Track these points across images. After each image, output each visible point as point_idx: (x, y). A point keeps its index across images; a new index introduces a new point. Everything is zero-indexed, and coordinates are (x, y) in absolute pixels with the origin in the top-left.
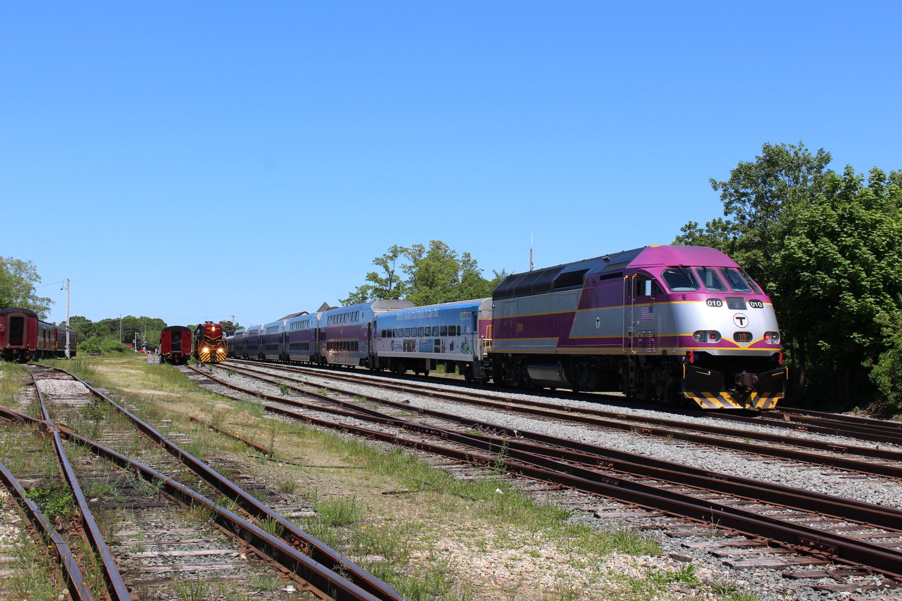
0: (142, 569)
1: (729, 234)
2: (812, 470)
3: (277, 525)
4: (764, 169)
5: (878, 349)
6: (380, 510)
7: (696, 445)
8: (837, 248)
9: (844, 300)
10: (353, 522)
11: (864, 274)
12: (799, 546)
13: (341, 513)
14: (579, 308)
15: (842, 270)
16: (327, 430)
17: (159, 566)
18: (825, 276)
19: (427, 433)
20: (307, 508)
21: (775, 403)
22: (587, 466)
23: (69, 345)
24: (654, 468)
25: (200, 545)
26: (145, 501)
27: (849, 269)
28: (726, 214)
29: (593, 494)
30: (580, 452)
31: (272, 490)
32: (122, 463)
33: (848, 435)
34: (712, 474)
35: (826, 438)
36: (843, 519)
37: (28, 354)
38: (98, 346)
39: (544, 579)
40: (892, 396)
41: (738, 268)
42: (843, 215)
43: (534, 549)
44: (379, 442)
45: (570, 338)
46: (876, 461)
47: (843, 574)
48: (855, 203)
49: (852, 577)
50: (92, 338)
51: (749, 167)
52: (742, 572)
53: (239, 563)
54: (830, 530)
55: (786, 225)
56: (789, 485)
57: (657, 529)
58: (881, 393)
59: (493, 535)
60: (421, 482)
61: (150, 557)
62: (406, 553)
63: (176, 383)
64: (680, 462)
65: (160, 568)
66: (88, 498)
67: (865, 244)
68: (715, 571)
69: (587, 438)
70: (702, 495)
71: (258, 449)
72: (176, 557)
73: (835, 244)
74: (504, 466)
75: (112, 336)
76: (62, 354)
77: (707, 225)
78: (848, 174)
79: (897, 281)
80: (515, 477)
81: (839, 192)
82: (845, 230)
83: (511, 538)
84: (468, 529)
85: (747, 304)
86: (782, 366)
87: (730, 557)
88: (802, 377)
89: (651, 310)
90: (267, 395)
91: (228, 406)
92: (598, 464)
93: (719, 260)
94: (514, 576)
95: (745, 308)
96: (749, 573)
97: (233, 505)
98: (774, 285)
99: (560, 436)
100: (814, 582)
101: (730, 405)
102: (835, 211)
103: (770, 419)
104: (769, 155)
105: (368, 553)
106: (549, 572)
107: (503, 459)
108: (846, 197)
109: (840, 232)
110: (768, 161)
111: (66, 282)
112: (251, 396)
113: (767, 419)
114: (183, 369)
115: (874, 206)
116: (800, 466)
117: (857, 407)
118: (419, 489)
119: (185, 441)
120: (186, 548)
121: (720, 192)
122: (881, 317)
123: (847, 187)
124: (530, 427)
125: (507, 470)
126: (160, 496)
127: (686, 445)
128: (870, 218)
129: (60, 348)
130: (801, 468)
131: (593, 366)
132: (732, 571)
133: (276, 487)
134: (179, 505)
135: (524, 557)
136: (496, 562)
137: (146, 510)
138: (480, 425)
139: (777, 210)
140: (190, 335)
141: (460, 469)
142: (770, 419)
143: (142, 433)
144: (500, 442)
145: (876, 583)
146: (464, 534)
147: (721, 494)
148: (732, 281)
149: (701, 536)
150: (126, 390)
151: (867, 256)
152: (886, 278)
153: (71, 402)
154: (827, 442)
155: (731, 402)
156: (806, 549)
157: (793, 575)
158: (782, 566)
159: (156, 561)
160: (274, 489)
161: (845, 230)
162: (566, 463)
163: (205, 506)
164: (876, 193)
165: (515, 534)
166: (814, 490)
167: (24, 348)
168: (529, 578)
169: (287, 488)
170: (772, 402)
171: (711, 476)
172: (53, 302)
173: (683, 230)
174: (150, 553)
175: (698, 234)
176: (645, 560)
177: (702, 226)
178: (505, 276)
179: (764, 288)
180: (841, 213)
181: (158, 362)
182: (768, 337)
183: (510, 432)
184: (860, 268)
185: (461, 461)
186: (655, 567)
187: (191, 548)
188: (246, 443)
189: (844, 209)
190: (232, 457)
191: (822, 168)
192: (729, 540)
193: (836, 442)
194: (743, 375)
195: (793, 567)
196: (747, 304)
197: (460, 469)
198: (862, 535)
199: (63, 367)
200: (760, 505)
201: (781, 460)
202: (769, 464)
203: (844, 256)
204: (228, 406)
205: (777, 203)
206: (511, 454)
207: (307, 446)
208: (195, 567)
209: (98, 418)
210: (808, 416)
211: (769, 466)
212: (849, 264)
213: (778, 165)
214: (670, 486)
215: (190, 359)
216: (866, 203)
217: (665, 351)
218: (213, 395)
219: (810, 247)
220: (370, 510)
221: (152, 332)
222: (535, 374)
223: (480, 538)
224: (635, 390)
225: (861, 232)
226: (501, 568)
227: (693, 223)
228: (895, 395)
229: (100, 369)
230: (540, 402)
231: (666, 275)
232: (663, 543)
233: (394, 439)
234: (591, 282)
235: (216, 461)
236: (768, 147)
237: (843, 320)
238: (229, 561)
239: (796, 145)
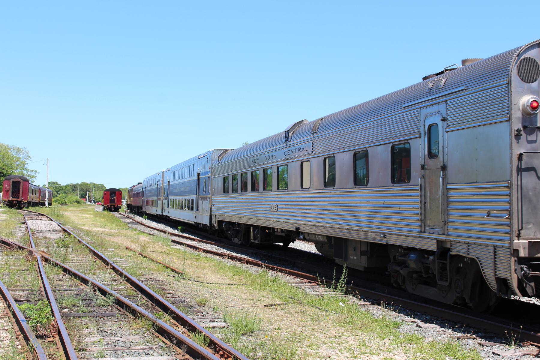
16: (213, 256)
23: (48, 199)
32: (85, 281)
37: (23, 204)
38: (65, 200)
44: (250, 266)
50: (61, 195)
63: (114, 224)
71: (173, 270)
76: (43, 204)
97: (166, 317)
111: (47, 160)
114: (116, 214)
119: (125, 264)
120: (136, 354)
129: (42, 201)
137: (102, 319)
150: (84, 228)
153: (48, 235)
167: (20, 200)
181: (102, 210)
190: (157, 276)
218: (138, 231)
221: (97, 192)
229: (67, 214)
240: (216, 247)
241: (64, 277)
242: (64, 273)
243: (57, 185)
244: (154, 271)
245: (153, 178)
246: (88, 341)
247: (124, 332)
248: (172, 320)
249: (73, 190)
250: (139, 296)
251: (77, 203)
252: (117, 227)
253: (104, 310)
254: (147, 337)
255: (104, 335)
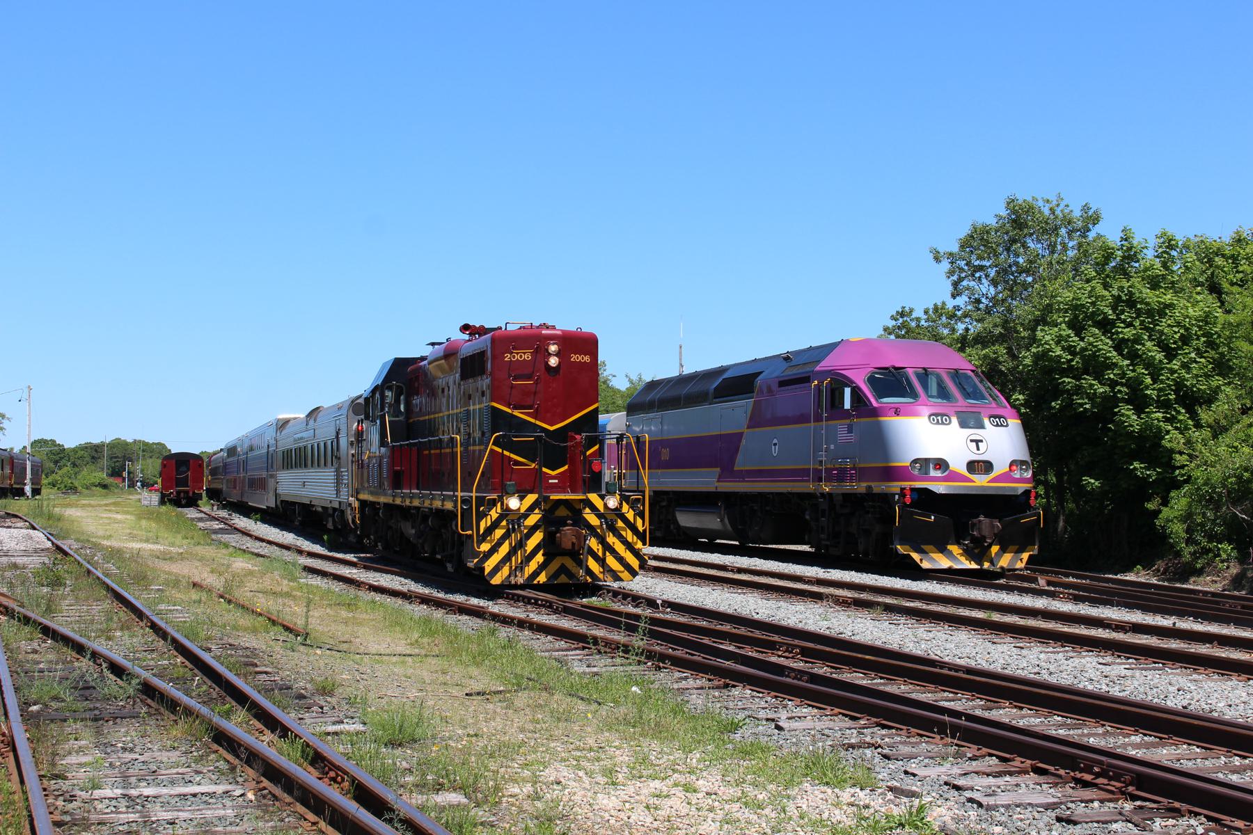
0: (94, 817)
1: (956, 324)
2: (1084, 657)
3: (303, 747)
4: (1007, 233)
5: (1168, 485)
6: (462, 720)
7: (917, 620)
8: (1111, 343)
9: (1121, 416)
10: (420, 740)
11: (1150, 380)
12: (1077, 773)
13: (401, 726)
14: (748, 428)
15: (1119, 374)
16: (389, 600)
17: (121, 813)
18: (1093, 382)
19: (533, 603)
20: (352, 718)
21: (1025, 560)
22: (762, 652)
23: (31, 479)
24: (860, 656)
25: (187, 778)
26: (111, 709)
27: (1128, 372)
28: (954, 296)
29: (773, 693)
30: (752, 632)
31: (303, 691)
32: (80, 649)
33: (1130, 607)
34: (942, 665)
35: (1100, 610)
36: (1137, 731)
38: (74, 481)
39: (704, 827)
40: (1187, 551)
41: (973, 371)
42: (1119, 296)
43: (688, 780)
44: (465, 618)
45: (735, 469)
46: (1174, 644)
47: (1146, 817)
48: (1136, 281)
49: (1158, 821)
50: (65, 470)
51: (986, 231)
52: (997, 814)
53: (243, 807)
54: (1119, 747)
55: (1039, 310)
56: (1053, 680)
57: (868, 747)
58: (1172, 546)
59: (627, 758)
60: (522, 677)
61: (109, 798)
62: (497, 789)
63: (179, 533)
64: (895, 647)
65: (122, 816)
66: (25, 705)
67: (1150, 337)
68: (957, 811)
69: (760, 611)
70: (929, 695)
71: (287, 629)
72: (148, 797)
73: (1109, 338)
74: (642, 654)
75: (93, 467)
76: (20, 493)
77: (926, 312)
78: (1126, 240)
79: (1195, 389)
80: (658, 668)
81: (1113, 264)
82: (1123, 317)
83: (654, 762)
84: (591, 749)
85: (986, 421)
86: (1035, 509)
87: (977, 790)
88: (1061, 524)
89: (850, 431)
90: (307, 549)
91: (250, 566)
92: (779, 650)
93: (947, 360)
94: (658, 822)
95: (982, 427)
96: (1006, 814)
97: (241, 714)
98: (1021, 397)
99: (723, 608)
100: (1104, 828)
101: (962, 563)
102: (1108, 290)
103: (1018, 584)
104: (1014, 212)
105: (439, 788)
106: (711, 815)
107: (641, 643)
108: (1122, 271)
109: (1116, 320)
110: (1014, 221)
111: (26, 391)
112: (284, 551)
113: (1013, 583)
114: (191, 513)
115: (1162, 284)
116: (1067, 651)
117: (1138, 567)
118: (519, 687)
119: (180, 618)
120: (164, 783)
121: (945, 265)
122: (1173, 439)
123: (1124, 258)
124: (680, 596)
125: (646, 658)
126: (134, 702)
127: (902, 621)
128: (1157, 301)
129: (18, 484)
130: (1069, 654)
131: (768, 508)
132: (982, 812)
133: (308, 686)
134: (160, 714)
135: (673, 792)
136: (632, 801)
137: (111, 723)
138: (608, 593)
139: (1025, 290)
140: (201, 466)
141: (579, 657)
142: (1018, 584)
143: (120, 605)
144: (637, 617)
145: (1195, 830)
146: (585, 757)
147: (957, 693)
148: (964, 389)
149: (932, 758)
150: (106, 543)
151: (1153, 354)
152: (1179, 385)
153: (20, 561)
154: (1102, 616)
155: (963, 559)
156: (1088, 777)
157: (1073, 818)
158: (1055, 803)
159: (117, 804)
160: (306, 689)
161: (1123, 317)
162: (731, 648)
163: (197, 717)
164: (1165, 265)
165: (659, 756)
166: (1090, 687)
168: (681, 826)
169: (324, 688)
170: (1021, 560)
171: (942, 668)
172: (8, 419)
173: (893, 318)
174: (110, 791)
175: (913, 324)
176: (853, 796)
177: (918, 313)
178: (642, 385)
179: (1008, 399)
180: (1117, 294)
181: (157, 503)
182: (1014, 468)
183: (651, 603)
184: (1143, 371)
185: (581, 645)
186: (867, 807)
187: (173, 783)
188: (269, 619)
189: (1121, 289)
190: (248, 641)
191: (1088, 231)
192: (974, 763)
193: (1114, 617)
194: (980, 521)
195: (1070, 805)
196: (986, 421)
197: (579, 657)
198: (1166, 754)
199: (18, 511)
200: (1015, 710)
201: (1039, 642)
202: (1022, 648)
203: (1121, 354)
204: (250, 566)
205: (1025, 281)
206: (653, 635)
207: (361, 624)
208: (176, 813)
209: (57, 582)
210: (1071, 579)
211: (1023, 651)
212: (1128, 365)
213: (1027, 226)
214: (882, 681)
215: (201, 499)
216: (1152, 280)
217: (869, 487)
218: (231, 549)
219: (1073, 341)
220: (445, 720)
221: (150, 461)
222: (686, 520)
223: (608, 763)
224: (828, 543)
225: (1144, 321)
226: (639, 811)
227: (907, 309)
228: (1192, 549)
229: (71, 512)
230: (693, 559)
231: (872, 380)
232: (877, 769)
233: (485, 613)
234: (765, 391)
235: (224, 647)
236: (1013, 201)
237: (1119, 444)
238: (228, 802)
239: (1053, 198)
240: (403, 579)
241: (43, 645)
242: (45, 637)
243: (55, 446)
244: (246, 629)
245: (260, 433)
246: (73, 762)
247: (149, 745)
248: (254, 722)
249: (93, 458)
250: (197, 678)
251: (101, 489)
252: (185, 541)
253: (118, 705)
254: (195, 754)
255: (109, 751)
